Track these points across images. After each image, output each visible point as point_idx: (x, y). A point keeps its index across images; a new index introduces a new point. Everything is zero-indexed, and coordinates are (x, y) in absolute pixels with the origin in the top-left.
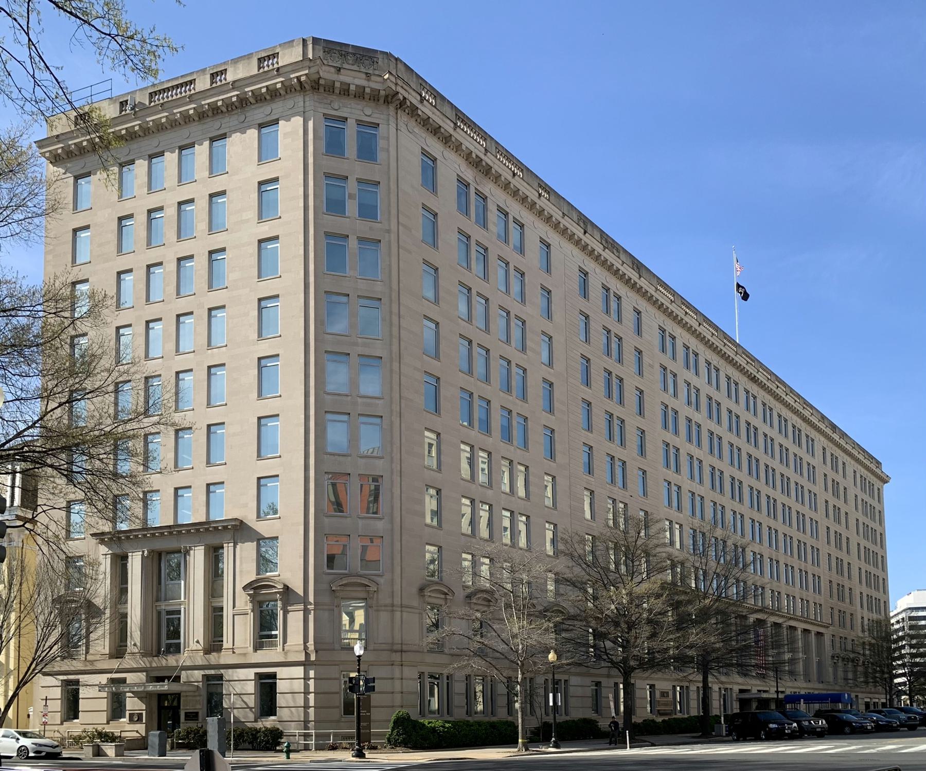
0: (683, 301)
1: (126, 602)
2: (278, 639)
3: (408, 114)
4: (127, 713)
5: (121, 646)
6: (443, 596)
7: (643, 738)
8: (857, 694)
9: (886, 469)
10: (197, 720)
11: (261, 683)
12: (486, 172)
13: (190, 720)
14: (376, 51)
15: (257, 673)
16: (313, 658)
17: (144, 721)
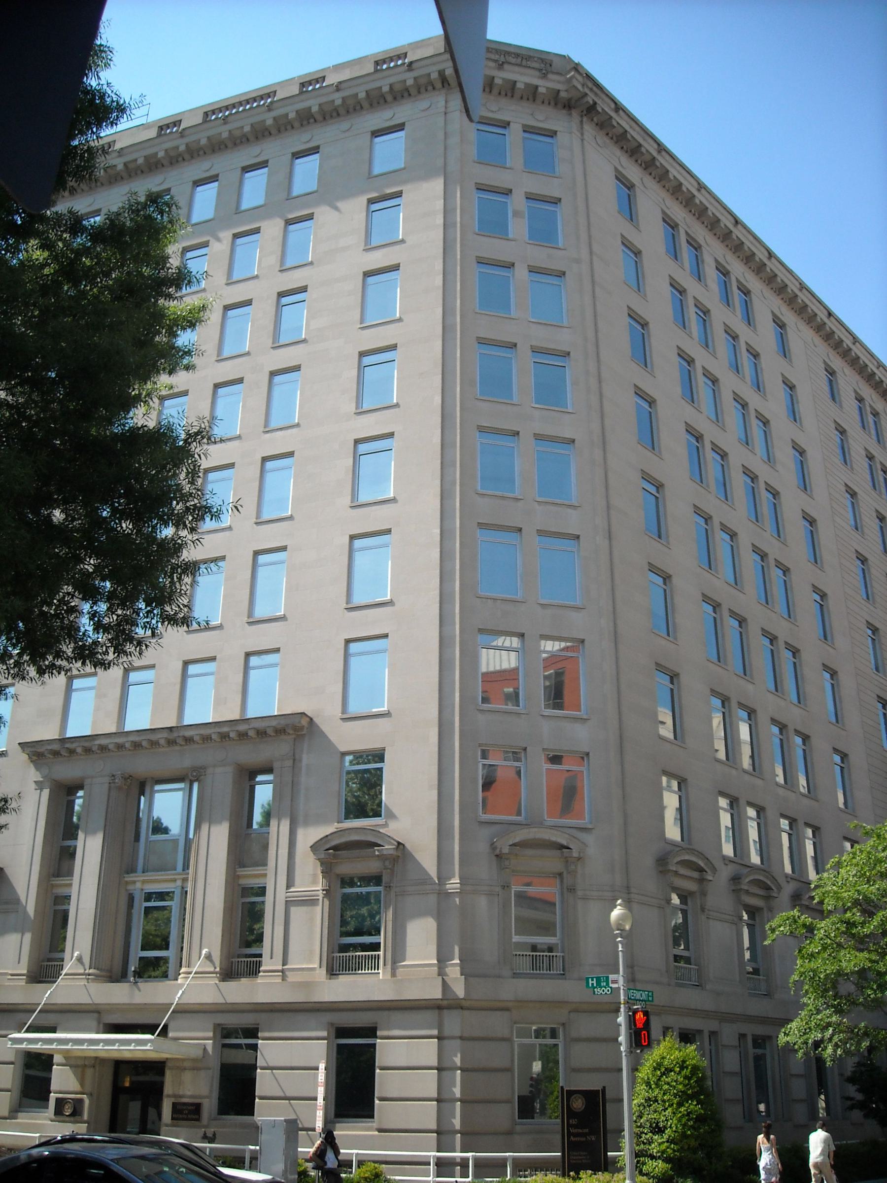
0: (828, 470)
1: (70, 873)
2: (381, 953)
3: (597, 124)
4: (53, 1096)
5: (49, 960)
6: (696, 875)
7: (30, 1109)
10: (198, 1120)
11: (340, 1046)
12: (699, 215)
13: (183, 1119)
15: (219, 1025)
16: (459, 990)
17: (86, 1117)
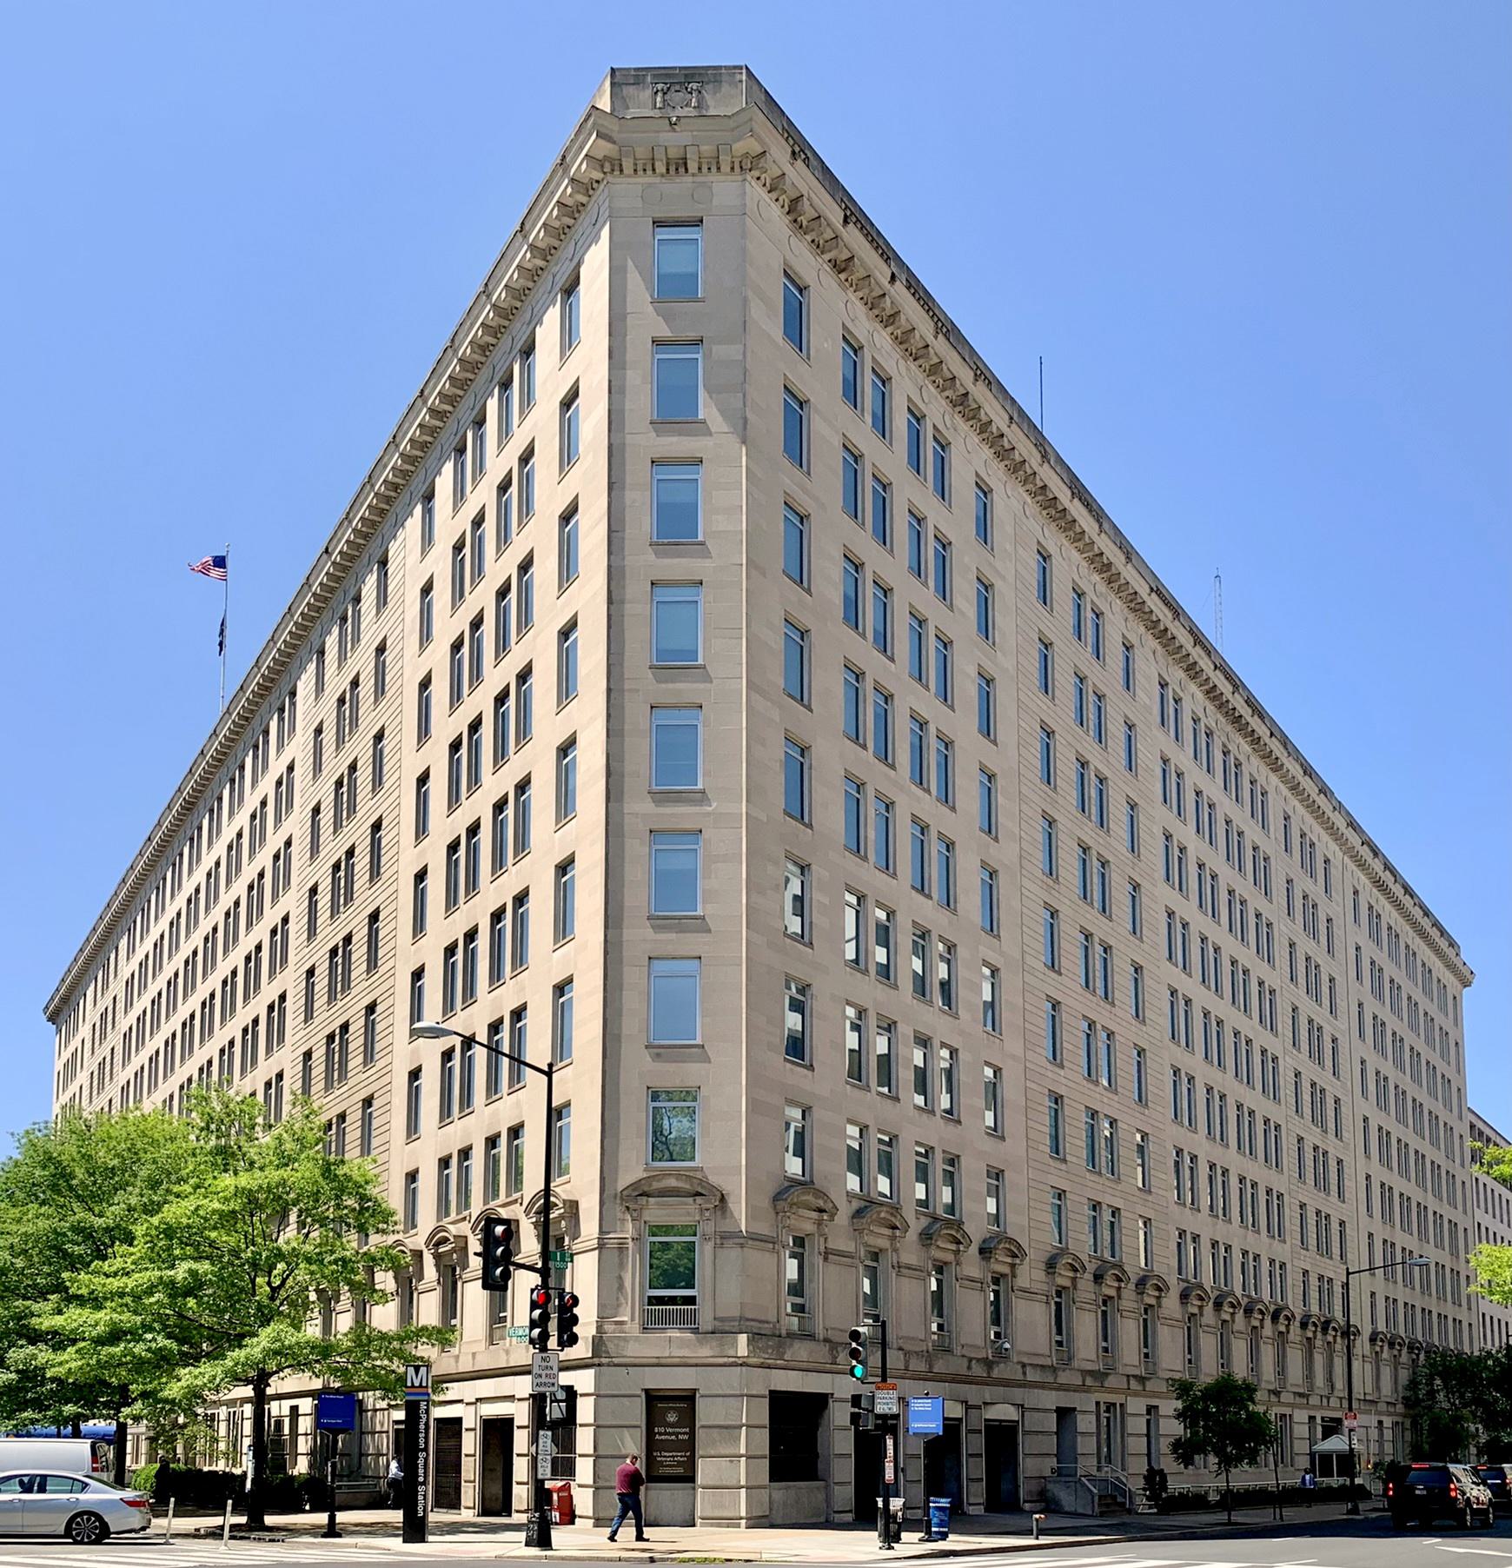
6: (888, 1232)
8: (1154, 1402)
9: (1469, 955)
14: (720, 67)
